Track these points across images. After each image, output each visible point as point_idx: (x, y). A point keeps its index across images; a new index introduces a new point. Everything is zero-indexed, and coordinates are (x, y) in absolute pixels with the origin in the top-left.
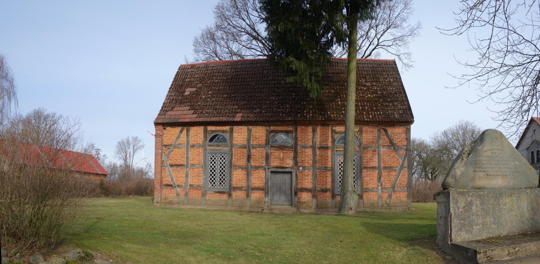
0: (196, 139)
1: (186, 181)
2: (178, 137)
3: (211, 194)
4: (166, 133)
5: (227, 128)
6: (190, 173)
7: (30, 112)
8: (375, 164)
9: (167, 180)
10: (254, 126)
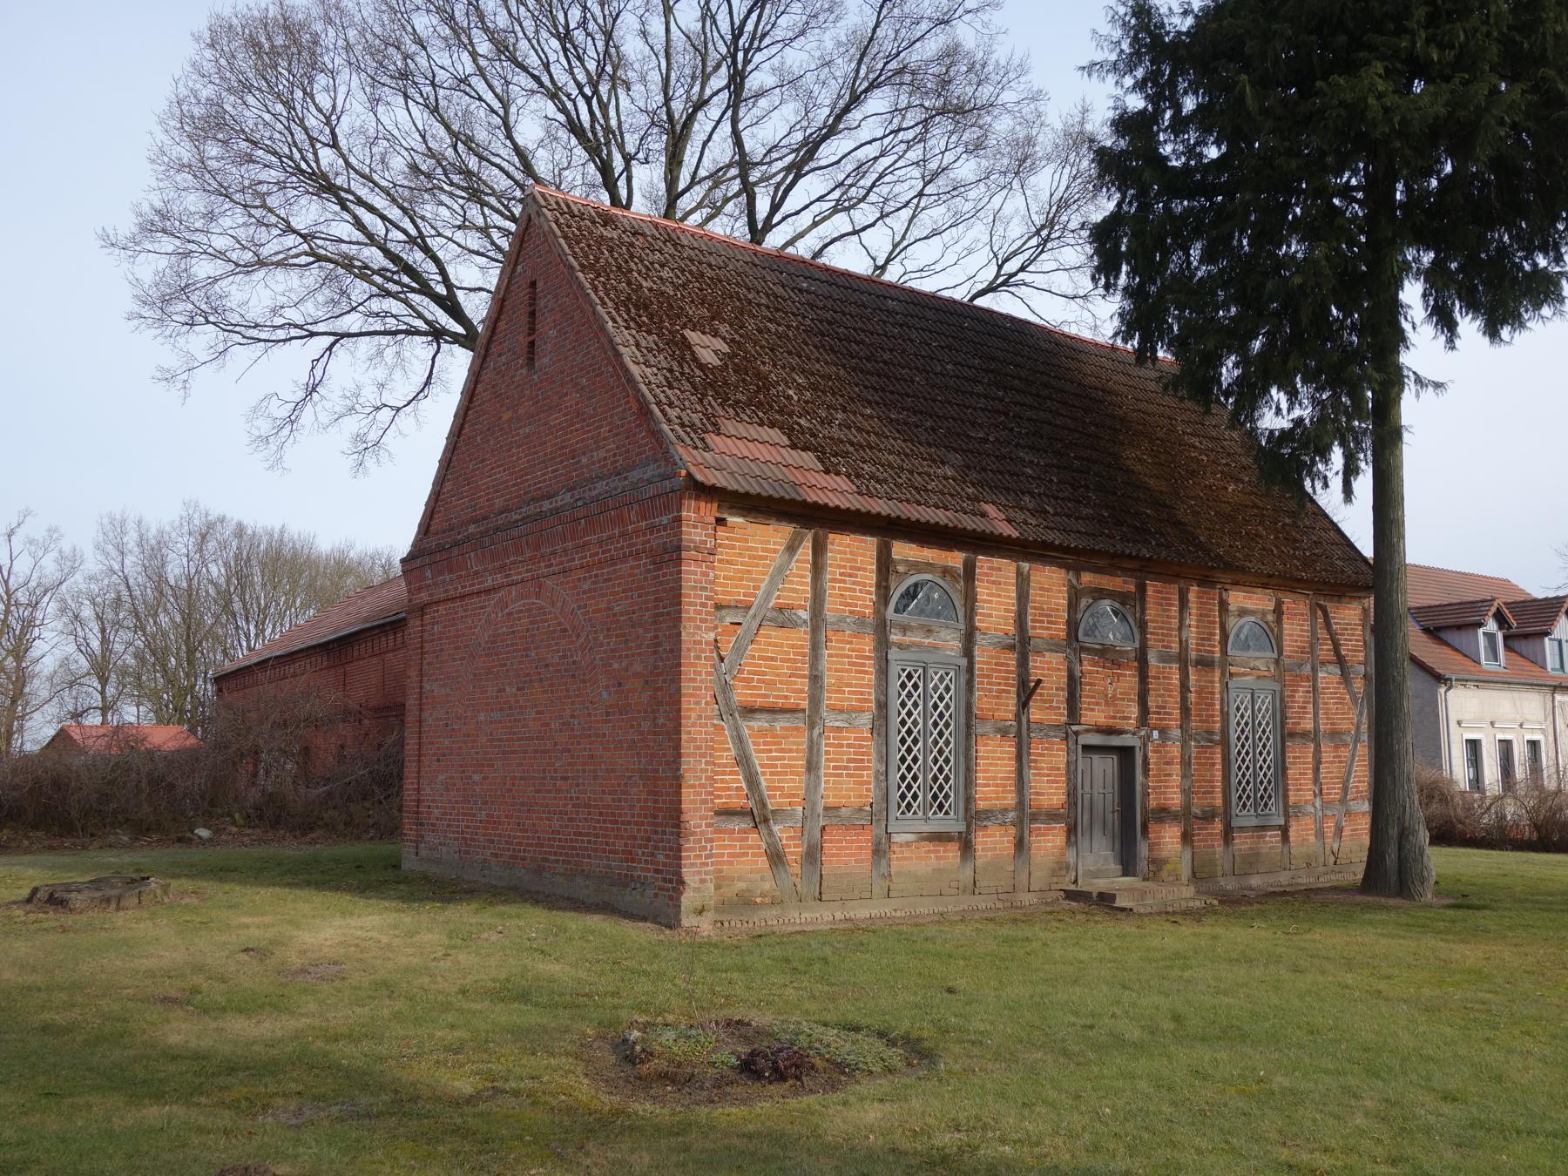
0: (850, 590)
1: (807, 789)
2: (780, 572)
3: (908, 844)
4: (727, 547)
5: (956, 559)
6: (827, 753)
7: (227, 12)
8: (1308, 725)
9: (729, 789)
10: (1036, 561)
